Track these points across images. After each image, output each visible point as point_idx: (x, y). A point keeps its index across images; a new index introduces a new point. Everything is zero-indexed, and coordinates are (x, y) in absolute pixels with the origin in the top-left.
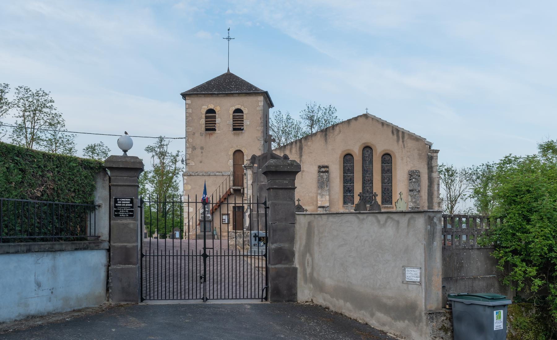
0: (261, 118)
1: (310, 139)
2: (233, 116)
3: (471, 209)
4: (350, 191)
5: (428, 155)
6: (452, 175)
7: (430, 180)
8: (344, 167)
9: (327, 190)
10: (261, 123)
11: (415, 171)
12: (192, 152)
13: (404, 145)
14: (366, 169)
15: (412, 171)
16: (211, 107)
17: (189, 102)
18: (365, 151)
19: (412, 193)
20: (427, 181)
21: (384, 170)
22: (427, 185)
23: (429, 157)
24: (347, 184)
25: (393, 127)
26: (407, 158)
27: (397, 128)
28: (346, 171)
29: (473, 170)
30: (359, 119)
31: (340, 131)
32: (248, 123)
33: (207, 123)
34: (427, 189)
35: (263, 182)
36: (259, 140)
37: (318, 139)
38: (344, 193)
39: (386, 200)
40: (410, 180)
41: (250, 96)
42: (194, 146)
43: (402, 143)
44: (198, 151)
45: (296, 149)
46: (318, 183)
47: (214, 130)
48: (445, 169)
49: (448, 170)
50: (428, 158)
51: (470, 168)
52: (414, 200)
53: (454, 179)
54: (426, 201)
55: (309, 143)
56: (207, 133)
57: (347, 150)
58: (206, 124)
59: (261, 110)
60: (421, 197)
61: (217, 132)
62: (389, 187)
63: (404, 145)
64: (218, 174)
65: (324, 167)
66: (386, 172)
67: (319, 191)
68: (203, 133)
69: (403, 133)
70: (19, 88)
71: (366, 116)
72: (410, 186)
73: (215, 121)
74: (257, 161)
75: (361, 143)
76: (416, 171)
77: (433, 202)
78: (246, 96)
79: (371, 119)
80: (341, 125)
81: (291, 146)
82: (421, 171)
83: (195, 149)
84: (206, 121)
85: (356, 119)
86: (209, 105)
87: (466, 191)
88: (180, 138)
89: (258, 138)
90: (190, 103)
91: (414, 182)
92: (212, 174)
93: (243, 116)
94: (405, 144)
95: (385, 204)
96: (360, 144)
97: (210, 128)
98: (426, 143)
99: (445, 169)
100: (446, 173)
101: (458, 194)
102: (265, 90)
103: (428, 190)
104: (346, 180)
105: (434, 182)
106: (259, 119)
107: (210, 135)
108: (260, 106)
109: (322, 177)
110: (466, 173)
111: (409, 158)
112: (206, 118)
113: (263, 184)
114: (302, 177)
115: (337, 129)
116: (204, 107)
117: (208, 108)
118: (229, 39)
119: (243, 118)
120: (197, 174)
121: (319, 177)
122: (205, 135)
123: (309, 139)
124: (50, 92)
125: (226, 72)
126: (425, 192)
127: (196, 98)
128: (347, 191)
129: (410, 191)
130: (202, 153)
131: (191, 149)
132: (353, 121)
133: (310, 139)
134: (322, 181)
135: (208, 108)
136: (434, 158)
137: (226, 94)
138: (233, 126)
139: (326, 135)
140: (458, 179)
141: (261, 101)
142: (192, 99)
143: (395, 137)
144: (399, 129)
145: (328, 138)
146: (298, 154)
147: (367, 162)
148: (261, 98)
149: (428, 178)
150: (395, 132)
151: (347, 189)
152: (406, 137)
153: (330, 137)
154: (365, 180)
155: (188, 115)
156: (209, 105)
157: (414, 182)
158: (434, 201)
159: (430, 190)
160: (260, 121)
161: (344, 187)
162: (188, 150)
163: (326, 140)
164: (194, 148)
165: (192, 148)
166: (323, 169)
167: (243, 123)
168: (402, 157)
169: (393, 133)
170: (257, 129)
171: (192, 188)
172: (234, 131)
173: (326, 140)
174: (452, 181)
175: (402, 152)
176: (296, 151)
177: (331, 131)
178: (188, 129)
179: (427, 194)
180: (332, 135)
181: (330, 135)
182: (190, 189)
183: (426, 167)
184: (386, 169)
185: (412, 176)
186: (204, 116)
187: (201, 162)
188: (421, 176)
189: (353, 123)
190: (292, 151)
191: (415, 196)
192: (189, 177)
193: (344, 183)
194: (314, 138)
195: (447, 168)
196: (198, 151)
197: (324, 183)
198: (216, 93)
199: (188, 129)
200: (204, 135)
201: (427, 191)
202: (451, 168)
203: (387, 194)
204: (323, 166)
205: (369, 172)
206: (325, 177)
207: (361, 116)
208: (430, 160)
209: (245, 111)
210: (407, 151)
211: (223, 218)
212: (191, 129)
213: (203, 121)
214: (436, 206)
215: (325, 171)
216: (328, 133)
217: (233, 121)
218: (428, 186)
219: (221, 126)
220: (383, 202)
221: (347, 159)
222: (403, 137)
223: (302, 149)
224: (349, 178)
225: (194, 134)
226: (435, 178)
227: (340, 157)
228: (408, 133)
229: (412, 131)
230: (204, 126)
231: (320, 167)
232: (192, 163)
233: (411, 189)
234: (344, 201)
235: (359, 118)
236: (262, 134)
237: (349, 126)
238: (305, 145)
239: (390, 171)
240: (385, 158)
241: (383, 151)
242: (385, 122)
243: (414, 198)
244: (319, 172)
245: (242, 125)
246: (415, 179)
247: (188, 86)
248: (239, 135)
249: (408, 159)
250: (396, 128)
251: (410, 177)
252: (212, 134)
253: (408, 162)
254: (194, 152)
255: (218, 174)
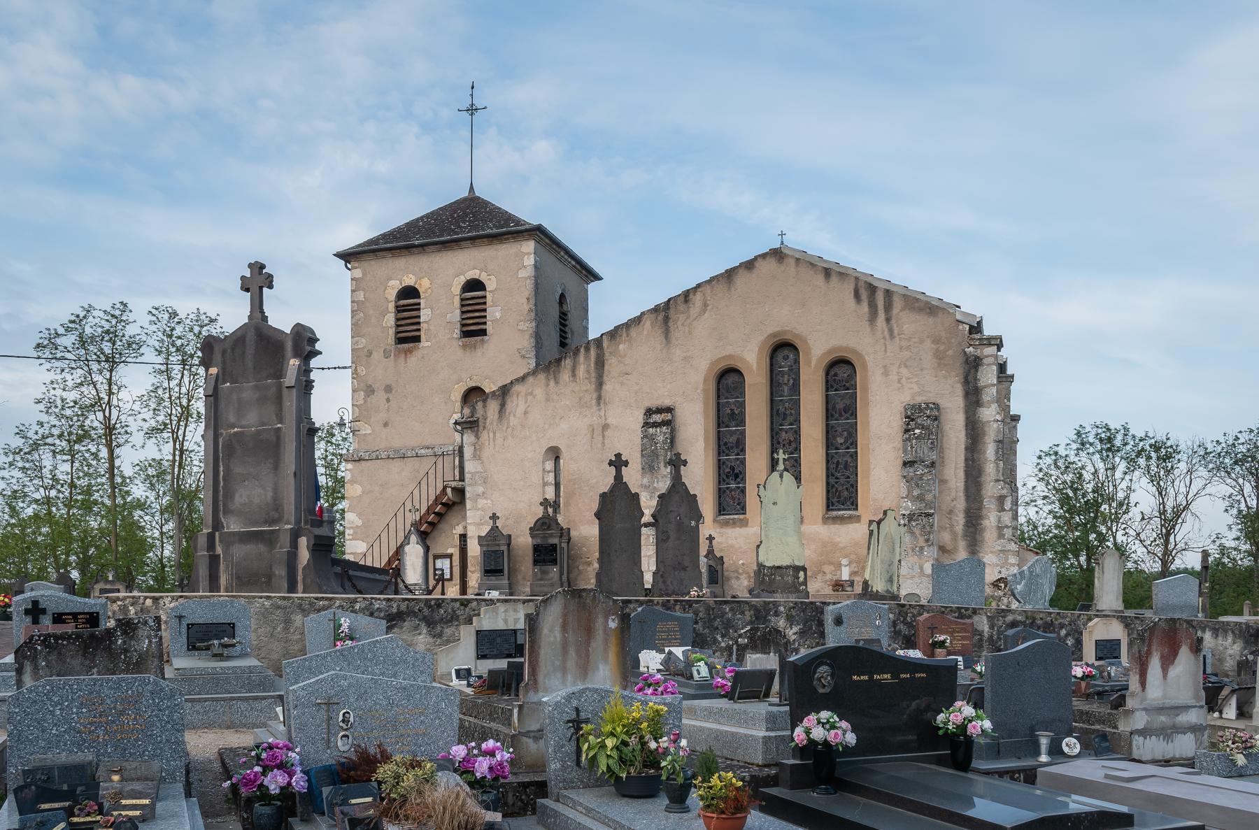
0: (528, 299)
1: (625, 335)
2: (462, 300)
3: (1220, 536)
4: (736, 476)
5: (965, 352)
6: (1168, 457)
7: (973, 429)
8: (719, 408)
9: (665, 476)
10: (530, 310)
11: (923, 406)
12: (365, 401)
13: (891, 331)
14: (782, 409)
15: (913, 406)
16: (410, 281)
17: (358, 273)
18: (780, 356)
19: (911, 470)
20: (963, 433)
21: (834, 408)
22: (963, 446)
23: (967, 359)
24: (727, 455)
25: (857, 278)
26: (900, 367)
27: (870, 280)
28: (726, 420)
29: (1224, 445)
30: (757, 264)
31: (705, 305)
32: (498, 315)
33: (399, 323)
34: (963, 458)
35: (233, 426)
36: (523, 357)
37: (645, 333)
38: (719, 482)
39: (839, 497)
40: (906, 431)
41: (501, 242)
42: (371, 386)
43: (884, 324)
44: (380, 396)
45: (589, 366)
46: (642, 455)
47: (417, 339)
48: (1151, 446)
49: (1156, 447)
50: (967, 362)
51: (1218, 441)
52: (915, 493)
53: (1172, 467)
54: (961, 495)
55: (621, 347)
56: (399, 352)
57: (724, 357)
58: (398, 326)
59: (529, 277)
60: (943, 482)
61: (424, 343)
62: (849, 460)
63: (891, 331)
64: (423, 451)
65: (659, 411)
66: (841, 415)
67: (645, 481)
68: (391, 351)
69: (888, 294)
70: (154, 311)
71: (778, 254)
72: (905, 451)
73: (419, 317)
74: (217, 357)
75: (766, 336)
76: (927, 404)
77: (981, 496)
78: (491, 244)
79: (792, 262)
80: (708, 289)
81: (575, 358)
82: (943, 403)
83: (373, 392)
84: (398, 320)
85: (749, 265)
86: (405, 278)
87: (1202, 494)
88: (339, 368)
89: (523, 352)
90: (361, 275)
91: (916, 438)
92: (409, 454)
93: (485, 297)
94: (895, 326)
95: (839, 510)
96: (761, 338)
97: (407, 335)
98: (959, 317)
99: (1151, 446)
100: (1153, 454)
101: (1184, 503)
102: (535, 223)
103: (966, 460)
104: (726, 444)
105: (984, 434)
106: (525, 301)
107: (406, 354)
108: (525, 267)
109: (652, 438)
110: (1206, 453)
111: (906, 366)
112: (399, 312)
113: (236, 433)
114: (603, 443)
115: (697, 299)
116: (392, 283)
117: (401, 283)
118: (472, 110)
119: (485, 303)
120: (374, 455)
121: (645, 440)
122: (395, 355)
123: (621, 336)
124: (218, 315)
125: (465, 193)
126: (956, 468)
127: (373, 263)
128: (727, 477)
129: (905, 464)
130: (388, 400)
131: (362, 393)
132: (741, 271)
133: (625, 335)
134: (653, 451)
135: (401, 283)
136: (985, 361)
137: (443, 243)
138: (463, 325)
139: (666, 319)
140: (1183, 466)
141: (529, 254)
142: (365, 264)
143: (865, 308)
144: (875, 284)
145: (672, 329)
146: (593, 380)
147: (786, 388)
148: (529, 246)
149: (966, 426)
150: (864, 295)
151: (728, 470)
152: (898, 304)
153: (679, 323)
154: (779, 443)
155: (356, 308)
156: (405, 278)
157: (916, 438)
158: (984, 492)
159: (973, 461)
160: (526, 307)
161: (720, 465)
162: (356, 395)
163: (667, 334)
164: (370, 391)
165: (365, 392)
166: (657, 418)
167: (485, 317)
168: (885, 367)
169: (857, 296)
170: (520, 327)
171: (363, 492)
172: (463, 339)
173: (667, 334)
174: (1168, 472)
175: (886, 351)
176: (588, 372)
177: (682, 307)
178: (357, 342)
179: (961, 474)
180: (682, 317)
181: (679, 320)
182: (360, 496)
183: (959, 389)
184: (840, 406)
185: (913, 420)
186: (391, 306)
187: (386, 425)
188: (942, 418)
189: (741, 280)
190: (577, 373)
191: (921, 479)
192: (357, 464)
193: (719, 453)
194: (633, 332)
195: (1156, 442)
196: (380, 396)
197: (657, 456)
198: (417, 242)
199: (357, 342)
200: (392, 355)
201: (961, 464)
202: (1165, 440)
203: (842, 480)
204: (657, 408)
205: (790, 419)
206: (661, 438)
207: (763, 256)
208: (973, 371)
209: (491, 285)
210: (901, 348)
211: (437, 567)
212: (363, 342)
213: (390, 319)
214: (993, 507)
215: (663, 421)
216: (672, 312)
217: (463, 312)
218: (966, 449)
219: (432, 328)
220: (833, 505)
221: (727, 384)
222: (888, 307)
223: (603, 366)
224: (733, 439)
225: (370, 354)
226: (989, 422)
227: (705, 380)
228: (887, 287)
229: (915, 285)
230: (392, 332)
231: (649, 412)
232: (366, 429)
233: (909, 458)
234: (720, 504)
235: (760, 264)
236: (533, 340)
237: (729, 289)
238: (611, 353)
239: (851, 410)
240: (836, 375)
241: (829, 352)
242: (834, 267)
243: (917, 486)
244: (646, 425)
245: (483, 320)
246: (923, 428)
247: (356, 235)
248: (475, 348)
249: (904, 371)
250: (866, 282)
251: (908, 424)
252: (410, 351)
253: (904, 381)
254: (369, 399)
255: (423, 451)
